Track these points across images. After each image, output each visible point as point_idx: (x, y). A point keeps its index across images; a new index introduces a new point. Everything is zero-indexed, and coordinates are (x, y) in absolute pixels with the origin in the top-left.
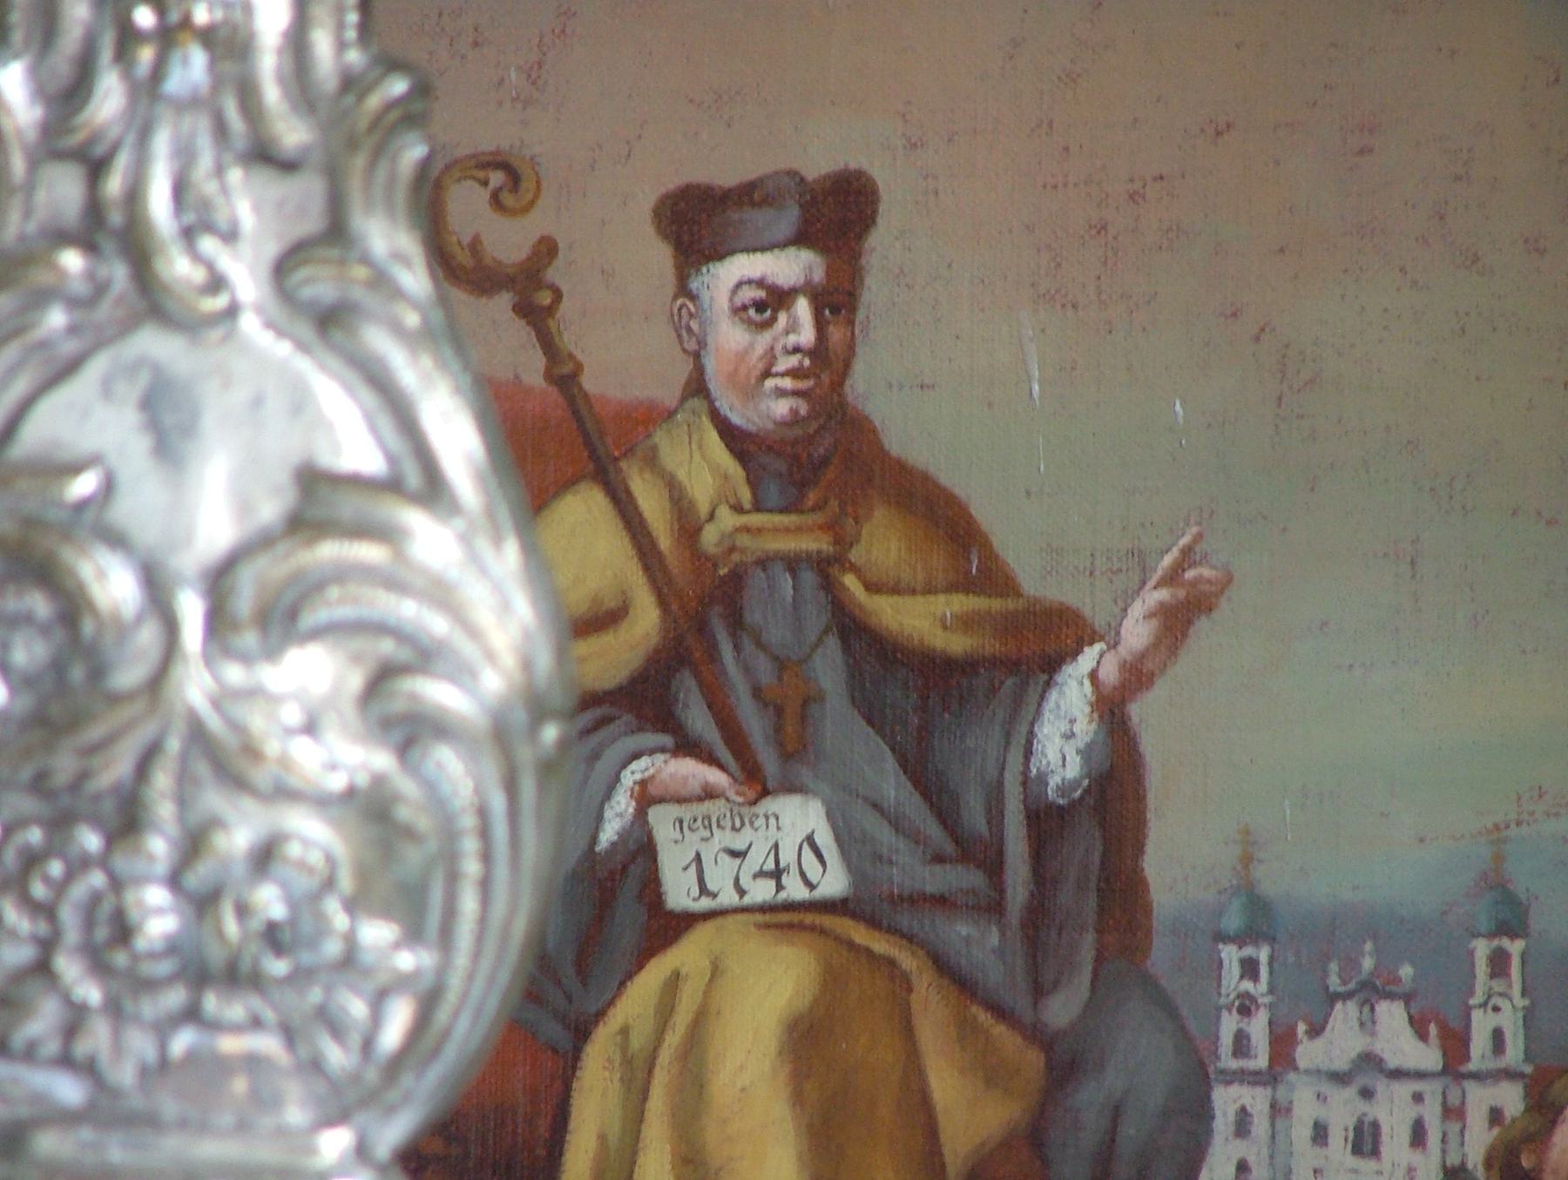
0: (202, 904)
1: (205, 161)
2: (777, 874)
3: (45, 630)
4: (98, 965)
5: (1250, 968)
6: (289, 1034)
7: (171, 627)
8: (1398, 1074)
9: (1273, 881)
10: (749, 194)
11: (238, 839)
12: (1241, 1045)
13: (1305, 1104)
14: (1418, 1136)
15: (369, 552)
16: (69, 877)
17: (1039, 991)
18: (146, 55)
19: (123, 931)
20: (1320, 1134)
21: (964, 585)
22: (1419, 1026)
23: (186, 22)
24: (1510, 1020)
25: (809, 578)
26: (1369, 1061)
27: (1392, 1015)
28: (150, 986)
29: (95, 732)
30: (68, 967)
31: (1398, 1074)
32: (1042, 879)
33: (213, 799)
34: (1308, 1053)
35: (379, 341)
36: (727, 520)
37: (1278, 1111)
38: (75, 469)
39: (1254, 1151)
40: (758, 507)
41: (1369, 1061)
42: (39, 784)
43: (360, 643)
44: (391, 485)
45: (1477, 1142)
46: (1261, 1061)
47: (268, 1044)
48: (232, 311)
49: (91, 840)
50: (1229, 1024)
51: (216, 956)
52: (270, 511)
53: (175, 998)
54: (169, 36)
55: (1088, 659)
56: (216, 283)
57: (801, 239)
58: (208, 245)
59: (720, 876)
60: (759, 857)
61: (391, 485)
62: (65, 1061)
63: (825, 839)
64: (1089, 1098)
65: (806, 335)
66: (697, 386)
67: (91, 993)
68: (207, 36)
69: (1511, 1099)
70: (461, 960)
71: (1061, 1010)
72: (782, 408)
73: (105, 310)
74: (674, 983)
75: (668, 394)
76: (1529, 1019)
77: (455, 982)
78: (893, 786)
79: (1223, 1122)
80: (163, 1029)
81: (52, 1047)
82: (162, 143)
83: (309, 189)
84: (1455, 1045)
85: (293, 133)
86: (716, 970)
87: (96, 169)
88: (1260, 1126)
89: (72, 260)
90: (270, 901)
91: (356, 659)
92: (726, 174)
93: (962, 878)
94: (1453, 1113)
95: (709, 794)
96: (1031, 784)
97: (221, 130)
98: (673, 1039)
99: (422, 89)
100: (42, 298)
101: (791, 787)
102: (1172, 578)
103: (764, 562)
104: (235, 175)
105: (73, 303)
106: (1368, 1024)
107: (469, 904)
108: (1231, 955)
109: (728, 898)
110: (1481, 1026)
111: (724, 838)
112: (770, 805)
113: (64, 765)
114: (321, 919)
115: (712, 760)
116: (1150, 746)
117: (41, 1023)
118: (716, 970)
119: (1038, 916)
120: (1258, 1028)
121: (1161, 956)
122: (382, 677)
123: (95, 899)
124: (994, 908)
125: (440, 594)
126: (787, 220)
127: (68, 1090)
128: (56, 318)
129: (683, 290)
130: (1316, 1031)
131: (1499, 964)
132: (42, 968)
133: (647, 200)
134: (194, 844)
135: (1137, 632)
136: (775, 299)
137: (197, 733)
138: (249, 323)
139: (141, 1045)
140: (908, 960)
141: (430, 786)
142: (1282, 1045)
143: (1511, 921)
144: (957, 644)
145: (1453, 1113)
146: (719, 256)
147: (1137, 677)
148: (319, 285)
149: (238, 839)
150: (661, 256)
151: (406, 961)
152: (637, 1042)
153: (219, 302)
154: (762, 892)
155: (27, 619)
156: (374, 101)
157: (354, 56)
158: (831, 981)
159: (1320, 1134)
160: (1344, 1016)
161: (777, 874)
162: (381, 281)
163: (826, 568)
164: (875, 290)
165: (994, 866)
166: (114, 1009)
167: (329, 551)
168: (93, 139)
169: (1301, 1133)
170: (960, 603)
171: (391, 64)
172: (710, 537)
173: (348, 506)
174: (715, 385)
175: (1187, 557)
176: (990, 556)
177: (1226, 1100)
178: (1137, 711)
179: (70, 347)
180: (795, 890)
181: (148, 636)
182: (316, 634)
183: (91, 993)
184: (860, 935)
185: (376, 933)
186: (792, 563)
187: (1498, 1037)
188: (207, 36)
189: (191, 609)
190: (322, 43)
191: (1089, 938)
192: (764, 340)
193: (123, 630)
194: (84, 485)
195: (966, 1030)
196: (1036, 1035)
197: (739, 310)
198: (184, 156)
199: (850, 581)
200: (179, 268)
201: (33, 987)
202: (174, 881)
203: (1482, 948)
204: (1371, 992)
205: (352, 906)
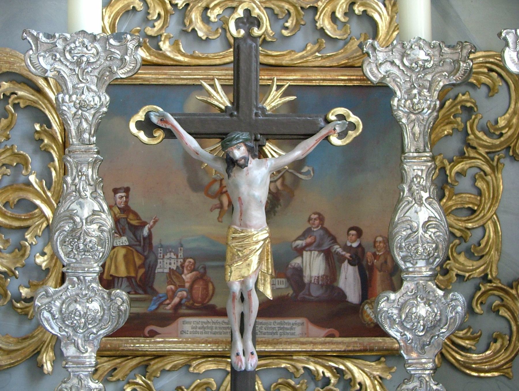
0: (86, 245)
1: (85, 185)
2: (123, 243)
3: (72, 223)
4: (77, 251)
5: (161, 250)
6: (92, 256)
7: (83, 223)
8: (173, 258)
9: (163, 243)
10: (120, 189)
11: (88, 240)
12: (160, 256)
13: (165, 261)
14: (174, 264)
15: (99, 217)
16: (74, 243)
17: (144, 251)
18: (80, 177)
19: (79, 248)
20: (167, 263)
21: (138, 220)
22: (174, 255)
23: (83, 174)
24: (182, 254)
25: (125, 219)
26: (170, 258)
27: (172, 254)
28: (81, 252)
29: (76, 232)
30: (74, 251)
31: (173, 258)
32: (144, 243)
33: (86, 237)
34: (166, 257)
35: (99, 199)
36: (118, 215)
37: (163, 261)
38: (74, 210)
39: (161, 265)
40: (121, 213)
41: (170, 258)
42: (72, 236)
43: (98, 224)
44: (100, 211)
45: (179, 264)
46: (162, 257)
47: (90, 257)
48: (87, 197)
49: (76, 240)
50: (159, 255)
51: (87, 250)
52: (90, 214)
53: (83, 253)
54: (82, 175)
55: (148, 225)
56: (86, 195)
57: (124, 192)
58: (85, 192)
59: (118, 243)
60: (121, 242)
61: (100, 211)
62: (74, 258)
63: (127, 240)
64: (148, 261)
65: (125, 200)
66: (116, 204)
67: (76, 253)
68: (85, 175)
69: (182, 260)
70: (106, 250)
71: (146, 253)
72: (123, 206)
73: (77, 198)
74: (114, 252)
75: (114, 205)
76: (183, 254)
77: (106, 251)
78: (132, 236)
79: (159, 262)
80: (82, 256)
81: (73, 257)
82: (81, 184)
83: (93, 187)
84: (177, 256)
85: (92, 183)
86: (118, 251)
87: (76, 186)
88: (162, 263)
89: (74, 193)
90: (91, 245)
91: (97, 225)
92: (118, 186)
93: (138, 243)
94: (177, 261)
95: (117, 237)
96: (143, 236)
97: (86, 183)
98: (114, 256)
99: (102, 179)
100: (71, 196)
101: (124, 236)
102: (154, 219)
103: (121, 218)
104: (87, 186)
105: (74, 197)
106: (170, 255)
107: (107, 245)
108: (159, 249)
109: (119, 245)
110: (179, 255)
111: (118, 240)
112: (122, 237)
113: (74, 234)
114: (95, 246)
115: (117, 234)
116: (153, 232)
117: (72, 255)
118: (118, 251)
119: (144, 246)
120: (162, 255)
121: (154, 249)
122: (100, 227)
123: (77, 245)
124: (140, 245)
125: (105, 220)
126: (123, 191)
127: (74, 261)
128: (73, 198)
129: (115, 196)
130: (166, 255)
131: (181, 249)
132: (72, 251)
133: (131, 187)
134: (85, 240)
135: (151, 223)
136: (122, 197)
137: (85, 231)
138: (89, 198)
139: (80, 257)
140: (133, 250)
141: (104, 236)
142: (163, 256)
143: (182, 246)
144: (137, 224)
145: (177, 261)
146: (117, 193)
147: (152, 227)
148: (94, 195)
149: (88, 240)
150: (113, 194)
151: (102, 250)
152: (112, 256)
153: (85, 197)
154: (121, 244)
155: (71, 222)
156: (99, 180)
157: (97, 177)
158: (127, 252)
159: (167, 263)
160: (168, 254)
161: (123, 243)
162: (99, 195)
163: (126, 218)
164: (130, 196)
165: (140, 242)
166: (78, 254)
167: (95, 217)
168: (76, 183)
169: (165, 263)
170: (138, 221)
171: (100, 178)
172: (117, 216)
173: (97, 213)
174: (117, 204)
175: (156, 217)
176: (140, 218)
177: (159, 261)
178: (152, 230)
179: (74, 200)
180: (124, 244)
181: (81, 224)
182: (94, 223)
183: (76, 253)
184: (129, 248)
185: (99, 248)
186: (124, 218)
187: (181, 256)
188: (85, 175)
189: (84, 221)
190: (94, 176)
191: (148, 248)
192: (121, 200)
193: (79, 223)
194: (75, 212)
195: (138, 256)
196: (143, 255)
197: (119, 198)
198: (83, 185)
199: (128, 220)
200: (83, 194)
201: (71, 252)
202: (83, 244)
203: (179, 248)
204: (170, 252)
205: (97, 245)
